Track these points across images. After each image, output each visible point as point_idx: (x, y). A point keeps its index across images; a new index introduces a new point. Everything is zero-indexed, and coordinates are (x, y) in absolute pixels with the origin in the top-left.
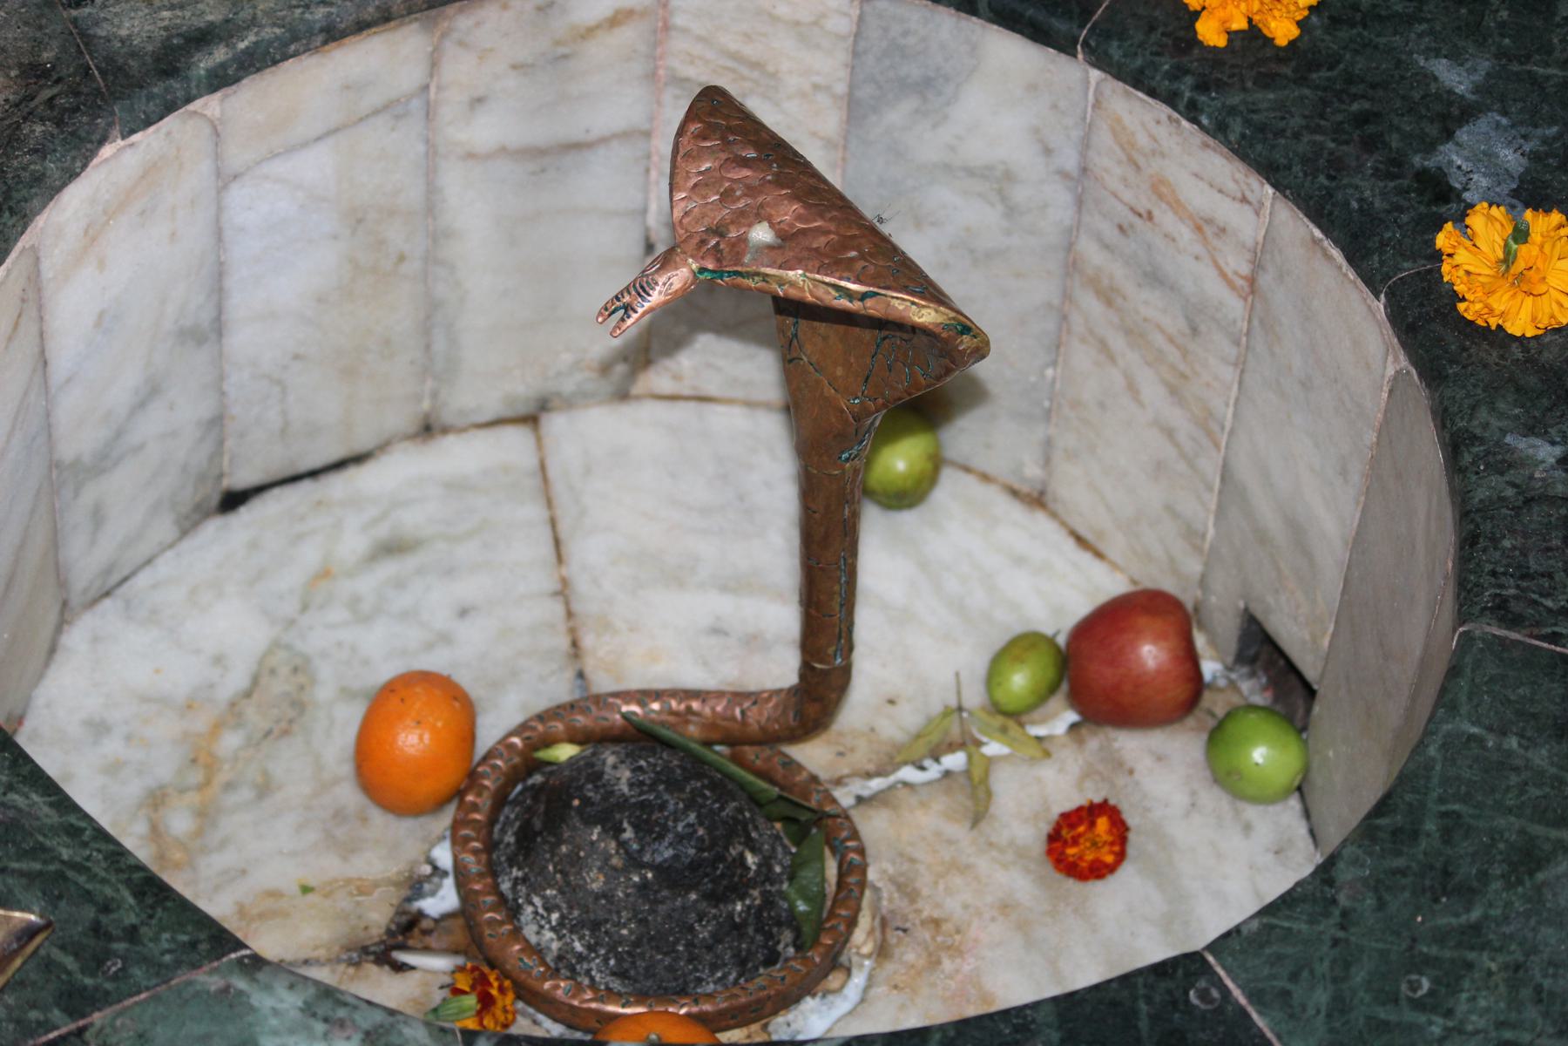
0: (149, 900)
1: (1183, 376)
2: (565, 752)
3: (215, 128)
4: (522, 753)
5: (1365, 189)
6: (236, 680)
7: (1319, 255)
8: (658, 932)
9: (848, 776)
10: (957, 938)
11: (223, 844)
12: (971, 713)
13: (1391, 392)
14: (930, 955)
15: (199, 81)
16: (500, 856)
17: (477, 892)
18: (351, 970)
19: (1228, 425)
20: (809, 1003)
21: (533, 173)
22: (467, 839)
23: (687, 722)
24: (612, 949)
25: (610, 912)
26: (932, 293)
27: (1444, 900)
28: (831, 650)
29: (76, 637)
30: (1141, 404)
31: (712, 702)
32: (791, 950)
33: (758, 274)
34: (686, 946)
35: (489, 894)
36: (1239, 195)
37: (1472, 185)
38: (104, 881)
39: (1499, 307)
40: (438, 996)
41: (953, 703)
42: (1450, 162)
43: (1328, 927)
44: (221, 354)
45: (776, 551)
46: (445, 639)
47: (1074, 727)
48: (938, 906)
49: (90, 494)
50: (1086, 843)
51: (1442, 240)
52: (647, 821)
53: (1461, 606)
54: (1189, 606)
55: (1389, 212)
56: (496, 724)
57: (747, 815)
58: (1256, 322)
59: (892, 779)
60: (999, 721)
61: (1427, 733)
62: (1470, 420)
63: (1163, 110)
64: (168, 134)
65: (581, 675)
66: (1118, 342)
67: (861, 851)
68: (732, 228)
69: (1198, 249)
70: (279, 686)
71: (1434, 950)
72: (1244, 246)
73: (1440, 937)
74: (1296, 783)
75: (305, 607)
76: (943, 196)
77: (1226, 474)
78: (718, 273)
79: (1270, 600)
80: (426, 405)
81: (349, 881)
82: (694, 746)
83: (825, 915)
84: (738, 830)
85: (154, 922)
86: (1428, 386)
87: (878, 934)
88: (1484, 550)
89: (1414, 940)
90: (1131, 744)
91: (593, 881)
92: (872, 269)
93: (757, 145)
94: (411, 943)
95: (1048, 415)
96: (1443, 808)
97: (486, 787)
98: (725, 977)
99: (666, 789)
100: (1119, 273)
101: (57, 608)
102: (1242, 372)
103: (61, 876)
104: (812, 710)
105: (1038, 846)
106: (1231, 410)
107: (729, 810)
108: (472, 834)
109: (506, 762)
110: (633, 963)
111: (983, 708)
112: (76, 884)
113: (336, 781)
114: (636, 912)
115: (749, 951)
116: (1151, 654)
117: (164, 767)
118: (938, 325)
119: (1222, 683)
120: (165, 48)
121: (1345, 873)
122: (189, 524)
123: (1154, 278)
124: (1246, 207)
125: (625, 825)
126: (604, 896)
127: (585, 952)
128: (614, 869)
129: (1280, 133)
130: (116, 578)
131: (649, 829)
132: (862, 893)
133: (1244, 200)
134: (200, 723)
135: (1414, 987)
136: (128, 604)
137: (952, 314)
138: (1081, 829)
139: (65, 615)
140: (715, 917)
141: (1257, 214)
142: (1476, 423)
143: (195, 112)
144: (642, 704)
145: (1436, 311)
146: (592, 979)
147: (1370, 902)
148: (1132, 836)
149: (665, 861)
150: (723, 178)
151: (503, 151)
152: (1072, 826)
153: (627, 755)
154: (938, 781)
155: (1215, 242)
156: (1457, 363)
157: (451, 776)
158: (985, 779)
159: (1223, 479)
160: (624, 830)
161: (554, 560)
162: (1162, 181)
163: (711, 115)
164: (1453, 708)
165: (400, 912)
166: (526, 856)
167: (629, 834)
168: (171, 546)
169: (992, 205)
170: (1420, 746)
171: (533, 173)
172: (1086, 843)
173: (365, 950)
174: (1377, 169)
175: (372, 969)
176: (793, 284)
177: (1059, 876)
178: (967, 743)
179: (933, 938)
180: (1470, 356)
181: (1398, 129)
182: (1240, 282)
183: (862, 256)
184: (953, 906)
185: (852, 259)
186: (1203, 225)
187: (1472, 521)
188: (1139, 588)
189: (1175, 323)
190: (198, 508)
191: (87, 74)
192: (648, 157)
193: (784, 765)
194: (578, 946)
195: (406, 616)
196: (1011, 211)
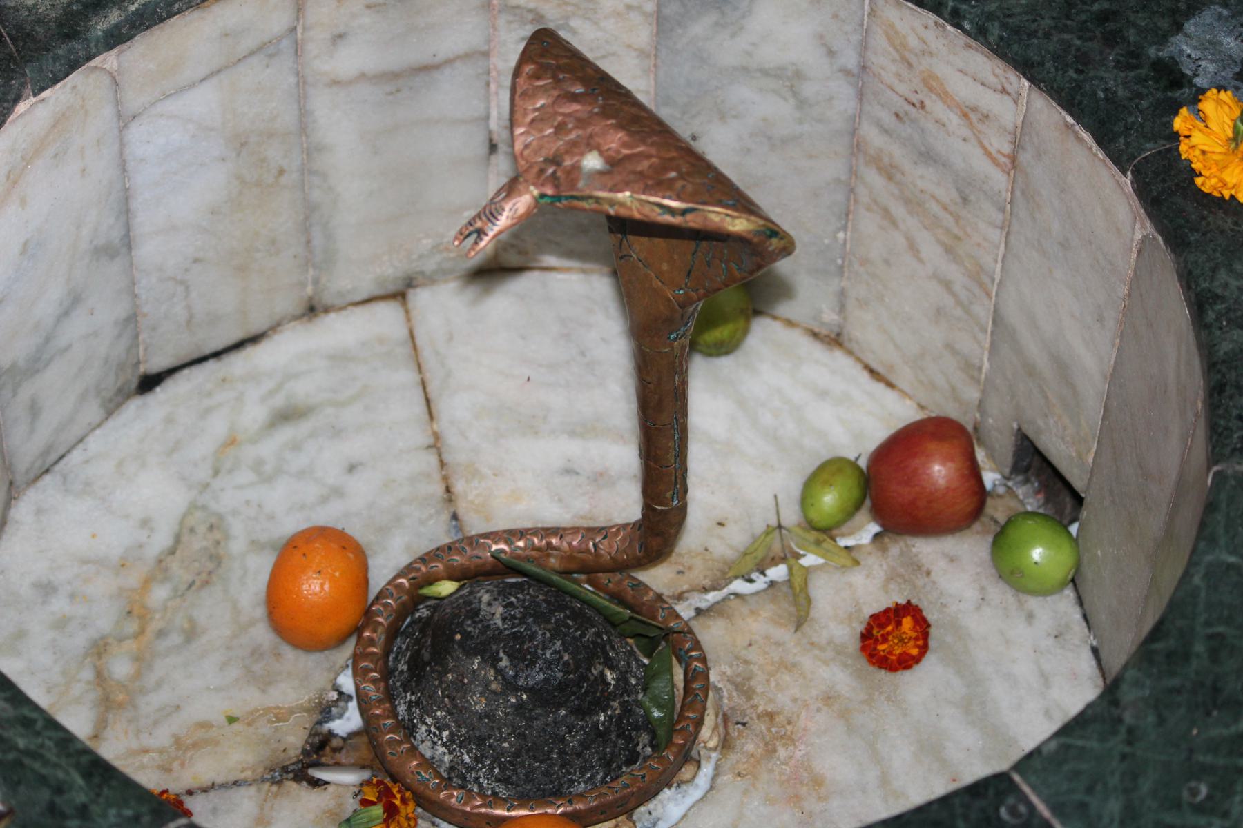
0: (96, 780)
1: (957, 238)
2: (446, 588)
3: (114, 78)
4: (408, 592)
5: (1110, 80)
6: (161, 540)
7: (1072, 137)
8: (534, 743)
9: (687, 591)
10: (789, 728)
11: (159, 684)
12: (788, 530)
13: (1139, 252)
14: (766, 744)
15: (98, 41)
17: (377, 717)
18: (274, 788)
20: (667, 793)
21: (391, 93)
22: (366, 671)
23: (549, 555)
24: (496, 759)
25: (492, 728)
26: (744, 205)
27: (1215, 713)
28: (669, 495)
29: (22, 511)
30: (921, 261)
31: (568, 538)
33: (591, 197)
34: (559, 754)
35: (388, 717)
36: (1000, 87)
37: (1201, 72)
38: (56, 766)
39: (1231, 181)
40: (351, 804)
41: (774, 522)
42: (1181, 52)
43: (1117, 744)
44: (131, 265)
45: (614, 397)
46: (337, 492)
47: (877, 536)
48: (771, 701)
49: (25, 394)
50: (894, 639)
51: (1179, 124)
52: (519, 651)
53: (1214, 448)
54: (970, 428)
55: (1131, 99)
56: (386, 565)
57: (605, 637)
58: (1018, 193)
59: (725, 591)
60: (813, 535)
61: (1192, 564)
62: (1212, 281)
63: (930, 17)
64: (74, 87)
65: (455, 517)
66: (899, 211)
67: (703, 660)
69: (965, 132)
70: (198, 543)
71: (1208, 759)
72: (1005, 130)
73: (1213, 747)
74: (1070, 577)
75: (216, 473)
76: (742, 93)
77: (997, 318)
78: (557, 197)
79: (1040, 423)
80: (309, 290)
81: (267, 710)
82: (555, 578)
83: (676, 717)
84: (597, 652)
85: (101, 800)
86: (1173, 251)
87: (721, 729)
88: (1231, 397)
89: (1191, 751)
90: (926, 549)
91: (476, 704)
92: (690, 188)
93: (583, 81)
94: (323, 760)
95: (841, 270)
96: (1210, 631)
97: (381, 624)
98: (593, 776)
99: (534, 622)
100: (897, 153)
101: (5, 488)
102: (1008, 233)
103: (18, 764)
104: (655, 543)
105: (854, 644)
106: (999, 265)
107: (589, 636)
108: (371, 666)
110: (515, 770)
111: (799, 525)
112: (32, 770)
113: (252, 623)
114: (514, 728)
115: (612, 753)
116: (940, 472)
117: (104, 620)
118: (750, 232)
119: (1001, 490)
120: (66, 14)
121: (1128, 694)
122: (112, 406)
123: (928, 156)
124: (1006, 97)
125: (501, 655)
128: (494, 692)
129: (1033, 34)
130: (53, 457)
132: (706, 696)
133: (1004, 91)
134: (133, 579)
135: (1194, 792)
137: (761, 222)
138: (889, 628)
139: (13, 492)
140: (582, 727)
141: (1016, 102)
142: (1216, 283)
143: (96, 67)
144: (507, 542)
145: (1177, 185)
146: (480, 786)
147: (1151, 718)
149: (537, 684)
150: (556, 113)
151: (362, 77)
152: (882, 626)
154: (764, 590)
155: (980, 127)
156: (1197, 231)
157: (350, 615)
159: (994, 322)
160: (501, 660)
161: (427, 417)
162: (933, 76)
163: (542, 56)
164: (1212, 541)
165: (313, 734)
166: (418, 683)
167: (504, 663)
168: (99, 426)
169: (786, 99)
170: (1186, 575)
171: (391, 93)
172: (894, 639)
173: (285, 769)
174: (1118, 62)
175: (292, 786)
176: (622, 204)
177: (871, 668)
178: (788, 557)
179: (769, 730)
180: (1208, 224)
181: (1134, 25)
182: (1003, 160)
183: (681, 176)
185: (672, 180)
186: (967, 112)
187: (1219, 371)
189: (947, 193)
190: (120, 391)
192: (488, 73)
193: (634, 587)
194: (467, 759)
195: (301, 474)
196: (802, 104)
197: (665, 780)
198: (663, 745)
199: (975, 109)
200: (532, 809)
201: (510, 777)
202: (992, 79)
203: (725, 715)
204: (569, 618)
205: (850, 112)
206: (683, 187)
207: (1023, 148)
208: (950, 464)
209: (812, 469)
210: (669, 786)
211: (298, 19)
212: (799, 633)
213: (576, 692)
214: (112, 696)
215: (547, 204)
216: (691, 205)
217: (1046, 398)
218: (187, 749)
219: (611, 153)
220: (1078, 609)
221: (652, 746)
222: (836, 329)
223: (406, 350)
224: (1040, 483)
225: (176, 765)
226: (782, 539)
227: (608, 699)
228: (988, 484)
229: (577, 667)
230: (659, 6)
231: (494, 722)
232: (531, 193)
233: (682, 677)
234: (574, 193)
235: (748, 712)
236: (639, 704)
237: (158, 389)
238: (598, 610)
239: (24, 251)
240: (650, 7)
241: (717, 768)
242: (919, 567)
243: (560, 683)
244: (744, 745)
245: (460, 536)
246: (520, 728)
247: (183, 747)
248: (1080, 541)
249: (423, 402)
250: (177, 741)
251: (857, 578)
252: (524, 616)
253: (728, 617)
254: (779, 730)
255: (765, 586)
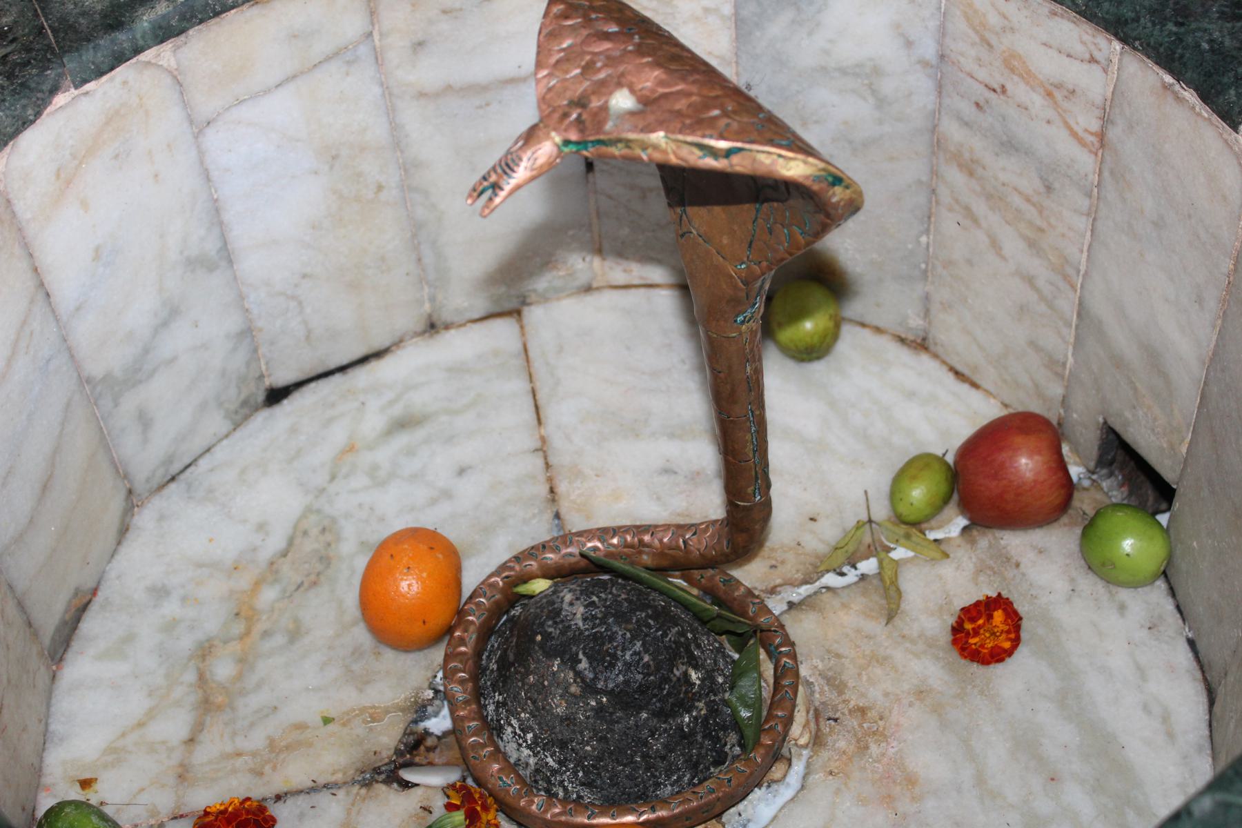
1: (1041, 230)
2: (540, 586)
3: (175, 77)
6: (276, 542)
7: (1170, 99)
9: (780, 585)
10: (881, 723)
11: (259, 686)
14: (858, 741)
16: (486, 681)
18: (363, 791)
19: (1083, 268)
20: (758, 793)
22: (456, 670)
23: (640, 553)
24: (579, 763)
28: (750, 490)
29: (145, 519)
30: (1004, 258)
32: (737, 750)
33: (619, 140)
35: (474, 719)
36: (1087, 56)
40: (439, 802)
41: (864, 517)
44: (235, 278)
46: (447, 494)
47: (965, 529)
48: (863, 695)
49: (130, 403)
50: (986, 633)
52: (599, 652)
54: (1055, 422)
57: (690, 635)
58: (1106, 174)
59: (817, 584)
60: (903, 529)
64: (125, 83)
65: (557, 516)
66: (980, 208)
67: (793, 656)
68: (593, 98)
69: (1050, 113)
70: (308, 546)
75: (333, 478)
77: (1082, 311)
79: (1128, 414)
80: (427, 307)
81: (363, 710)
82: (645, 575)
83: (765, 713)
84: (682, 652)
87: (813, 725)
90: (1015, 542)
91: (557, 706)
92: (735, 125)
93: (619, 22)
97: (472, 622)
98: (679, 779)
100: (978, 146)
102: (1094, 220)
104: (741, 539)
105: (946, 637)
106: (1085, 255)
108: (460, 666)
109: (488, 599)
110: (599, 774)
111: (889, 520)
114: (595, 732)
115: (699, 755)
117: (212, 621)
118: (807, 177)
119: (1086, 483)
123: (1010, 146)
124: (1094, 66)
125: (581, 656)
126: (567, 719)
127: (556, 766)
128: (573, 695)
131: (602, 658)
133: (1093, 60)
134: (244, 582)
136: (189, 486)
137: (822, 165)
138: (981, 622)
140: (665, 730)
141: (1105, 71)
143: (149, 63)
146: (565, 789)
148: (1025, 624)
153: (582, 591)
154: (856, 583)
155: (1065, 104)
157: (440, 616)
158: (894, 582)
159: (1079, 315)
160: (580, 661)
161: (536, 422)
166: (504, 682)
167: (584, 665)
168: (227, 436)
169: (865, 99)
171: (480, 107)
172: (986, 633)
173: (377, 771)
174: (1223, 13)
175: (381, 788)
176: (656, 147)
177: (963, 661)
178: (877, 549)
179: (861, 726)
183: (725, 114)
184: (875, 695)
185: (716, 118)
186: (1054, 91)
188: (1011, 411)
189: (1030, 183)
190: (245, 403)
191: (40, 33)
195: (415, 477)
196: (881, 102)
197: (757, 780)
198: (750, 747)
199: (1059, 86)
200: (613, 817)
201: (594, 781)
202: (1079, 49)
203: (816, 710)
204: (651, 617)
205: (930, 107)
206: (728, 125)
207: (1112, 123)
208: (1037, 458)
209: (900, 465)
210: (759, 785)
211: (373, 25)
212: (890, 626)
213: (659, 695)
214: (211, 698)
215: (572, 152)
216: (739, 145)
217: (1135, 389)
218: (281, 751)
219: (644, 92)
220: (1170, 600)
221: (740, 745)
222: (922, 334)
223: (521, 361)
224: (1124, 476)
225: (267, 769)
226: (872, 534)
227: (693, 700)
228: (1075, 478)
229: (658, 669)
230: (737, 7)
231: (575, 725)
232: (553, 139)
233: (772, 672)
234: (602, 137)
235: (840, 707)
236: (726, 703)
237: (285, 402)
238: (686, 606)
239: (97, 254)
240: (728, 9)
241: (808, 766)
242: (1008, 559)
243: (641, 685)
244: (835, 741)
245: (561, 533)
246: (601, 731)
247: (277, 749)
248: (1172, 531)
249: (533, 409)
250: (271, 744)
251: (947, 570)
252: (605, 616)
253: (820, 611)
254: (871, 727)
255: (856, 579)
